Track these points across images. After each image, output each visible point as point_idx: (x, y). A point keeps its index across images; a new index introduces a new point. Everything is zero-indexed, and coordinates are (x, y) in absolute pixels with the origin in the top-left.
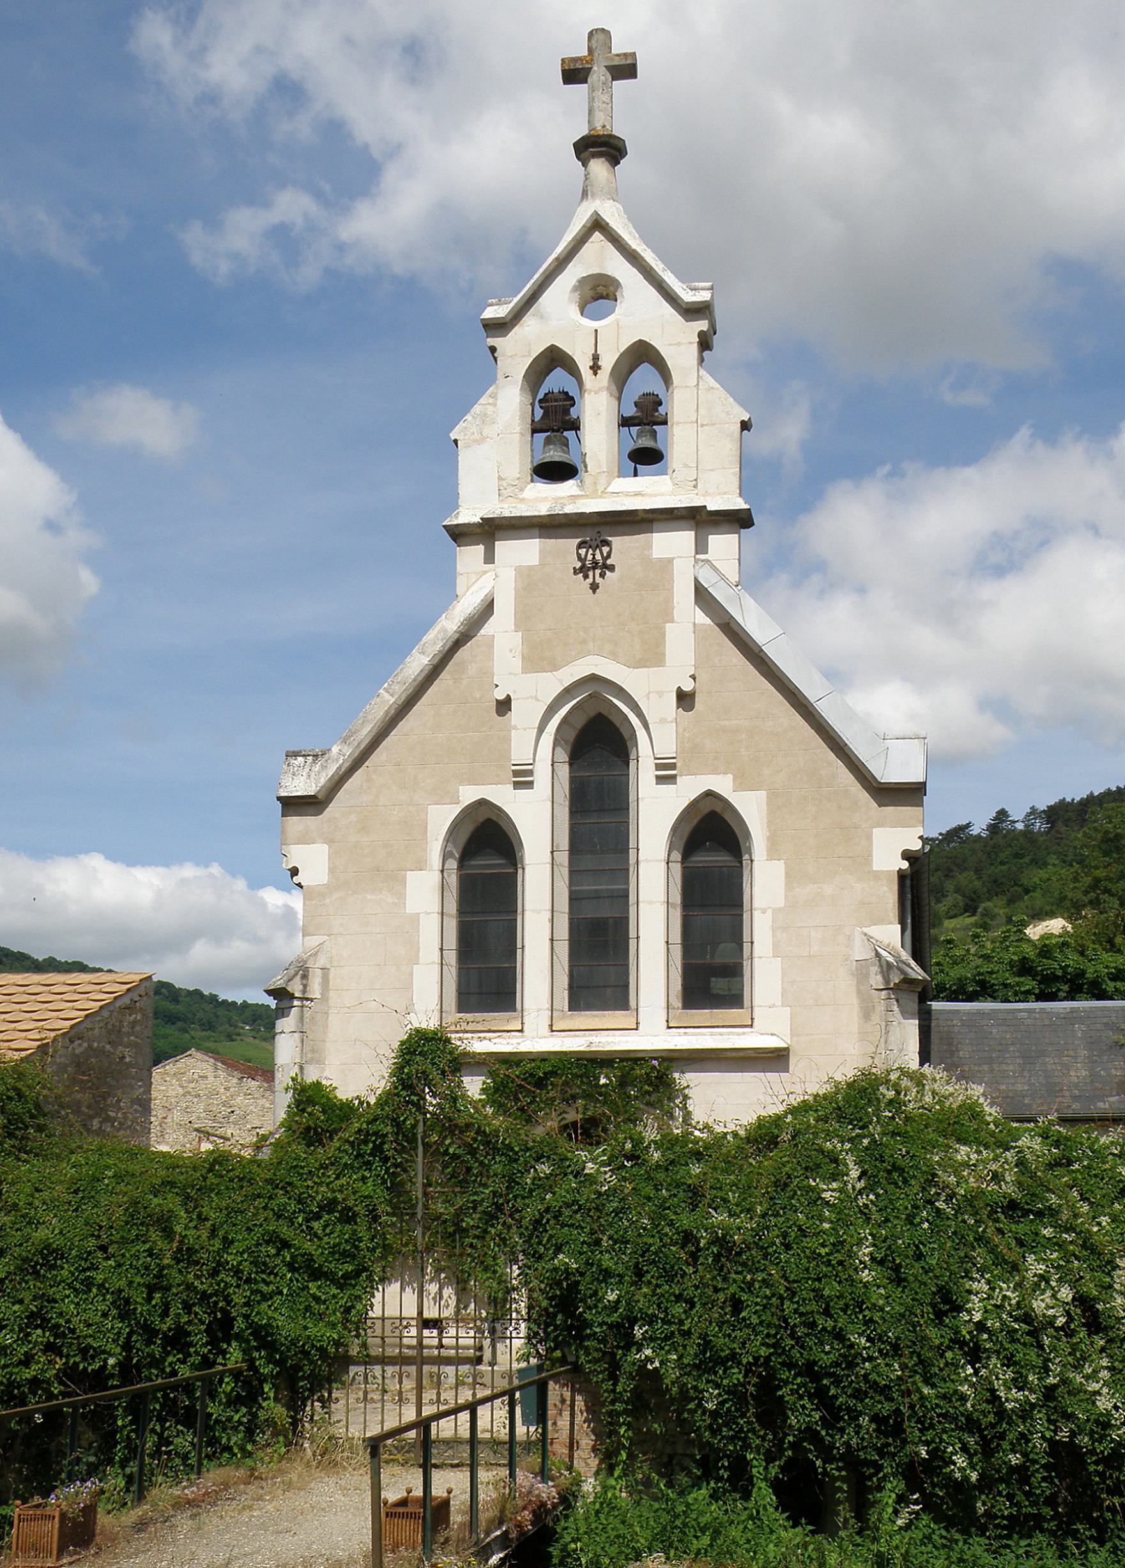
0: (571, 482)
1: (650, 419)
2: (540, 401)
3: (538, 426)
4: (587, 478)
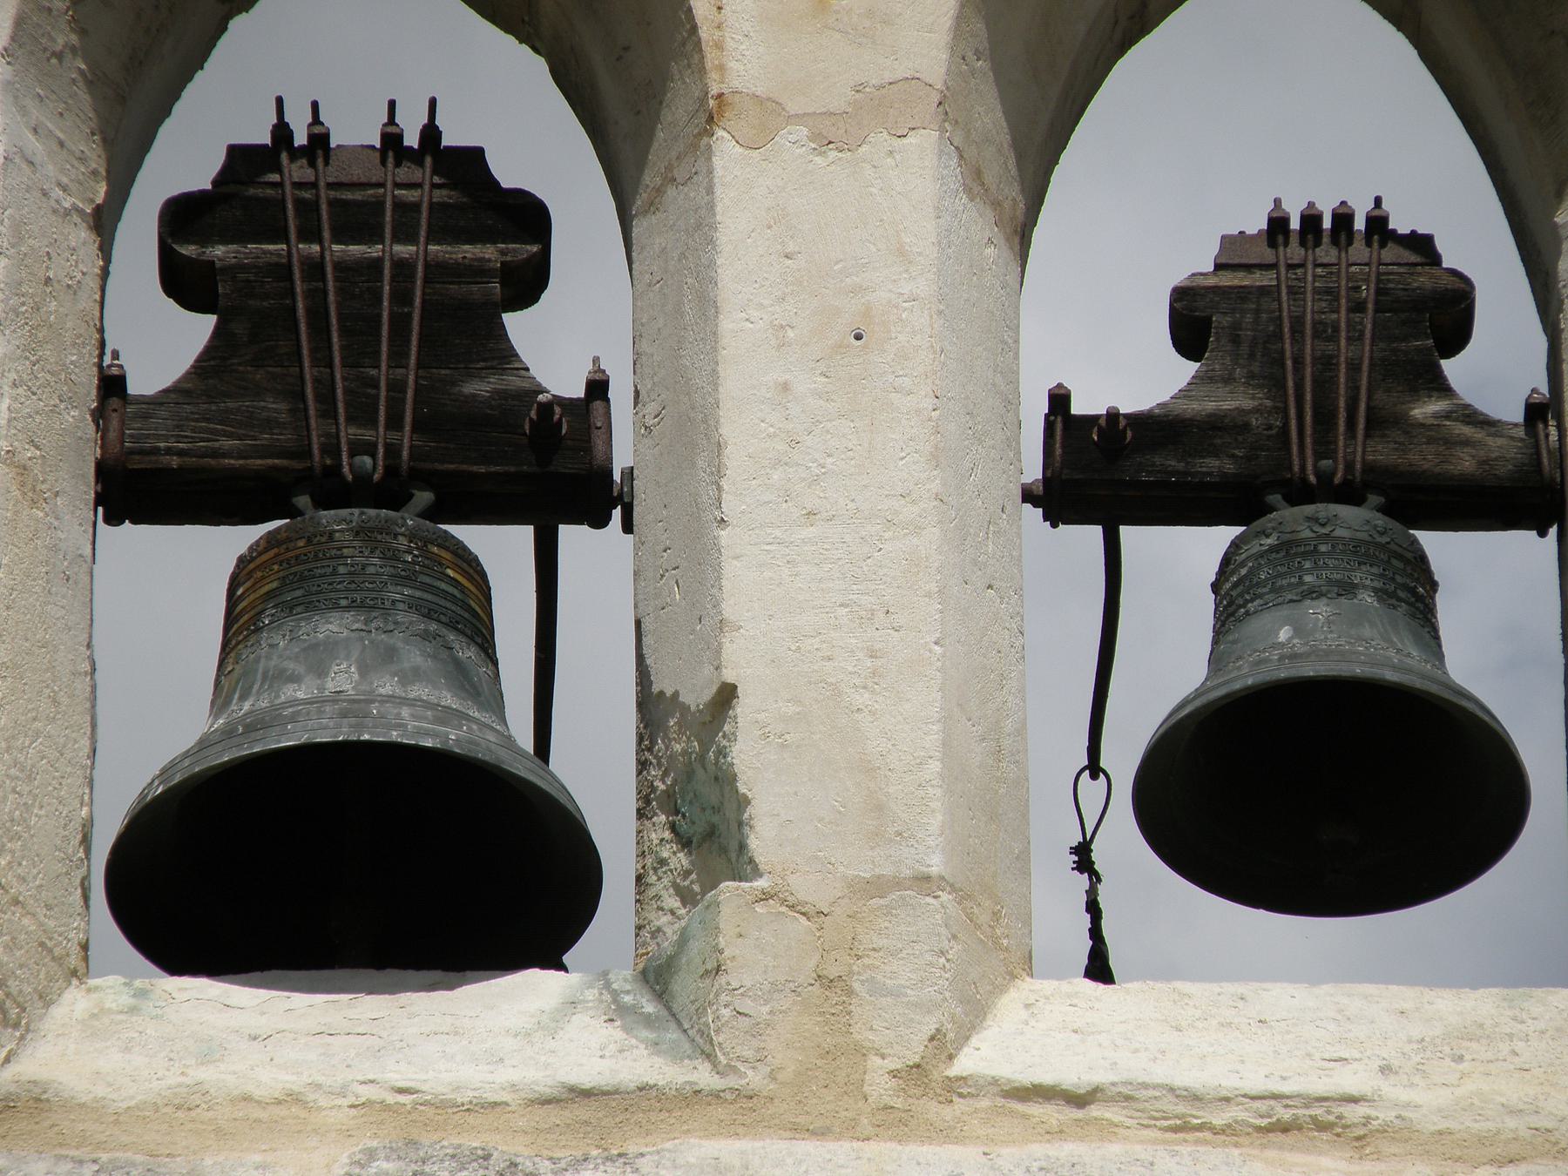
0: (529, 991)
1: (1359, 451)
2: (182, 216)
3: (170, 445)
4: (750, 939)
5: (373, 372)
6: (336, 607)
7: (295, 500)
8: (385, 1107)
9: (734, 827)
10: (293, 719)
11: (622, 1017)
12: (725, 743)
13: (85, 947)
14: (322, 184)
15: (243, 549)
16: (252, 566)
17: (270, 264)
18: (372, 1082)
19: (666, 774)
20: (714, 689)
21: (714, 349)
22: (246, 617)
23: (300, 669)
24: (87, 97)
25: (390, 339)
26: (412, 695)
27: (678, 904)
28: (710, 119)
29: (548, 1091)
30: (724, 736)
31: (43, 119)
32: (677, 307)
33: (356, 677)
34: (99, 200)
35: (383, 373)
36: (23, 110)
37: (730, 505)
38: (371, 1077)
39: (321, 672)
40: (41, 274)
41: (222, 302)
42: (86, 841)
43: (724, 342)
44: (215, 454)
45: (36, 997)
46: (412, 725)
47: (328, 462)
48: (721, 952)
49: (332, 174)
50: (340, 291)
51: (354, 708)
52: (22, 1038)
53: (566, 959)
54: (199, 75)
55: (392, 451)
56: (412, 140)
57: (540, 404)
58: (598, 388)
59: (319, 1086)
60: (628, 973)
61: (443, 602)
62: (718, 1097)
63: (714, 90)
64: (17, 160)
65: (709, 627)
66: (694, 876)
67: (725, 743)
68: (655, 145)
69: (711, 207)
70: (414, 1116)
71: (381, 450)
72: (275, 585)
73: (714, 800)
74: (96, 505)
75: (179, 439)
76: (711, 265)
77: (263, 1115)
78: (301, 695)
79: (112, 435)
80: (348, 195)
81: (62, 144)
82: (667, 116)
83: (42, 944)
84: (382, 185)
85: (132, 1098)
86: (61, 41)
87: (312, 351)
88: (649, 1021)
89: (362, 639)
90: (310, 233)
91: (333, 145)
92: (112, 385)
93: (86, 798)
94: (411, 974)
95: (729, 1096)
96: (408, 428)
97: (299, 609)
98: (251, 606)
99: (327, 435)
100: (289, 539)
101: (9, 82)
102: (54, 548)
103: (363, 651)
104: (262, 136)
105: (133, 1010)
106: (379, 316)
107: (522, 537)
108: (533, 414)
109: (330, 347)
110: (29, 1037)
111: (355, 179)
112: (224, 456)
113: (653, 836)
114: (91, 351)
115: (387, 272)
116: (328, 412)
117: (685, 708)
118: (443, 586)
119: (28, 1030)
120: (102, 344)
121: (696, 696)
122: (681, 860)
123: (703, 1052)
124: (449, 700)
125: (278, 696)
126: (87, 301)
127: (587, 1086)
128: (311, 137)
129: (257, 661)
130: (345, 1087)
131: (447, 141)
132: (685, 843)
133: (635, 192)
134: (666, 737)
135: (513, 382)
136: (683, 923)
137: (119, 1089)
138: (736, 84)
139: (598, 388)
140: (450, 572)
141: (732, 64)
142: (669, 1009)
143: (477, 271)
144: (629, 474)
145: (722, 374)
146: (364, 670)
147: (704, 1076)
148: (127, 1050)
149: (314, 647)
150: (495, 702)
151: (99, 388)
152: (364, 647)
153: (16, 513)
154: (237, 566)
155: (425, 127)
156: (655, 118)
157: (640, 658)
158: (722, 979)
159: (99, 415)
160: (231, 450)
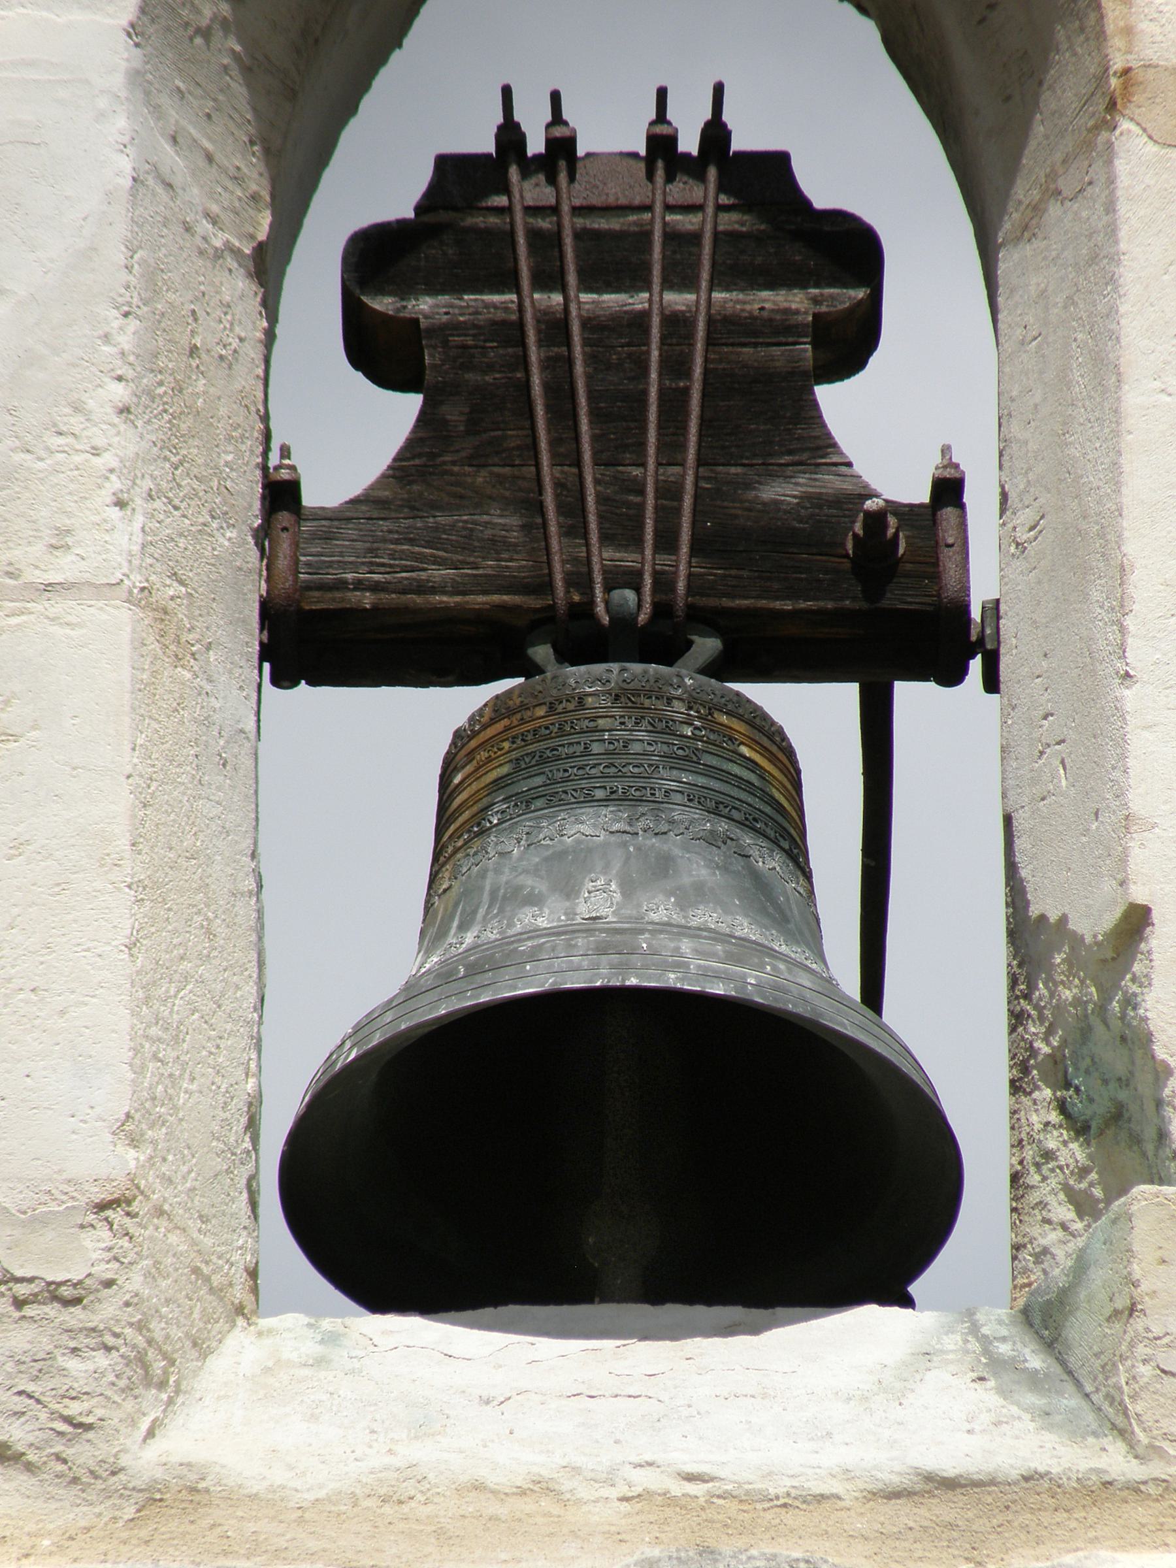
2: (376, 256)
3: (361, 577)
5: (636, 472)
6: (590, 800)
7: (531, 651)
8: (669, 1500)
9: (1150, 1107)
10: (533, 956)
11: (996, 1374)
12: (1134, 988)
13: (253, 1274)
14: (565, 208)
15: (460, 719)
16: (473, 744)
17: (494, 323)
18: (650, 1464)
19: (1050, 1032)
20: (1118, 912)
21: (1116, 434)
22: (467, 815)
23: (541, 886)
24: (243, 90)
25: (660, 427)
26: (695, 922)
27: (1072, 1215)
28: (1112, 106)
29: (896, 1479)
30: (1133, 980)
31: (184, 123)
32: (1062, 373)
33: (618, 897)
34: (262, 235)
35: (650, 473)
36: (157, 111)
37: (1138, 655)
38: (648, 1457)
39: (570, 891)
40: (184, 341)
41: (429, 376)
42: (252, 1125)
43: (1129, 423)
44: (422, 588)
45: (188, 1344)
46: (695, 964)
47: (576, 598)
48: (1136, 1284)
49: (579, 193)
50: (591, 359)
51: (616, 941)
52: (170, 1402)
53: (914, 1289)
54: (396, 56)
55: (664, 583)
56: (689, 143)
57: (868, 514)
58: (949, 489)
59: (576, 1470)
60: (1003, 1312)
61: (735, 792)
62: (1137, 1491)
63: (1118, 64)
64: (151, 181)
65: (1109, 824)
66: (1093, 1176)
67: (1134, 988)
68: (1032, 144)
69: (1112, 231)
70: (710, 1514)
71: (648, 581)
72: (505, 770)
73: (1121, 1069)
74: (262, 659)
75: (372, 567)
76: (1112, 313)
77: (502, 1511)
78: (542, 922)
79: (282, 563)
80: (601, 224)
81: (210, 158)
82: (1049, 101)
83: (196, 1271)
84: (648, 208)
85: (321, 1486)
86: (207, 12)
87: (554, 443)
88: (1034, 1381)
89: (625, 845)
90: (549, 277)
91: (580, 153)
92: (281, 495)
93: (253, 1065)
94: (700, 1312)
95: (1152, 1490)
96: (685, 549)
97: (539, 803)
98: (474, 798)
99: (575, 560)
100: (523, 707)
101: (138, 72)
102: (207, 722)
103: (628, 859)
104: (481, 141)
105: (320, 1362)
106: (645, 393)
107: (845, 697)
108: (858, 528)
109: (577, 439)
110: (180, 1400)
111: (611, 200)
112: (434, 590)
113: (1034, 1118)
114: (251, 447)
115: (655, 332)
116: (576, 528)
117: (1076, 940)
118: (736, 769)
119: (177, 1392)
120: (267, 436)
121: (1093, 921)
122: (1074, 1153)
123: (1114, 1426)
124: (746, 928)
125: (510, 925)
126: (246, 378)
127: (950, 1473)
128: (550, 142)
129: (483, 875)
130: (612, 1471)
131: (738, 144)
132: (1080, 1129)
133: (1003, 211)
134: (1049, 979)
135: (829, 483)
136: (1080, 1242)
137: (304, 1473)
138: (1150, 53)
139: (949, 489)
140: (745, 750)
141: (1144, 26)
142: (1063, 1363)
143: (779, 328)
144: (993, 609)
145: (1126, 468)
146: (628, 888)
147: (1116, 1461)
148: (314, 1418)
149: (561, 855)
150: (809, 932)
151: (263, 497)
152: (629, 856)
153: (154, 674)
154: (454, 743)
155: (708, 125)
156: (1031, 105)
157: (1011, 868)
158: (1138, 1323)
159: (263, 535)
160: (444, 583)
